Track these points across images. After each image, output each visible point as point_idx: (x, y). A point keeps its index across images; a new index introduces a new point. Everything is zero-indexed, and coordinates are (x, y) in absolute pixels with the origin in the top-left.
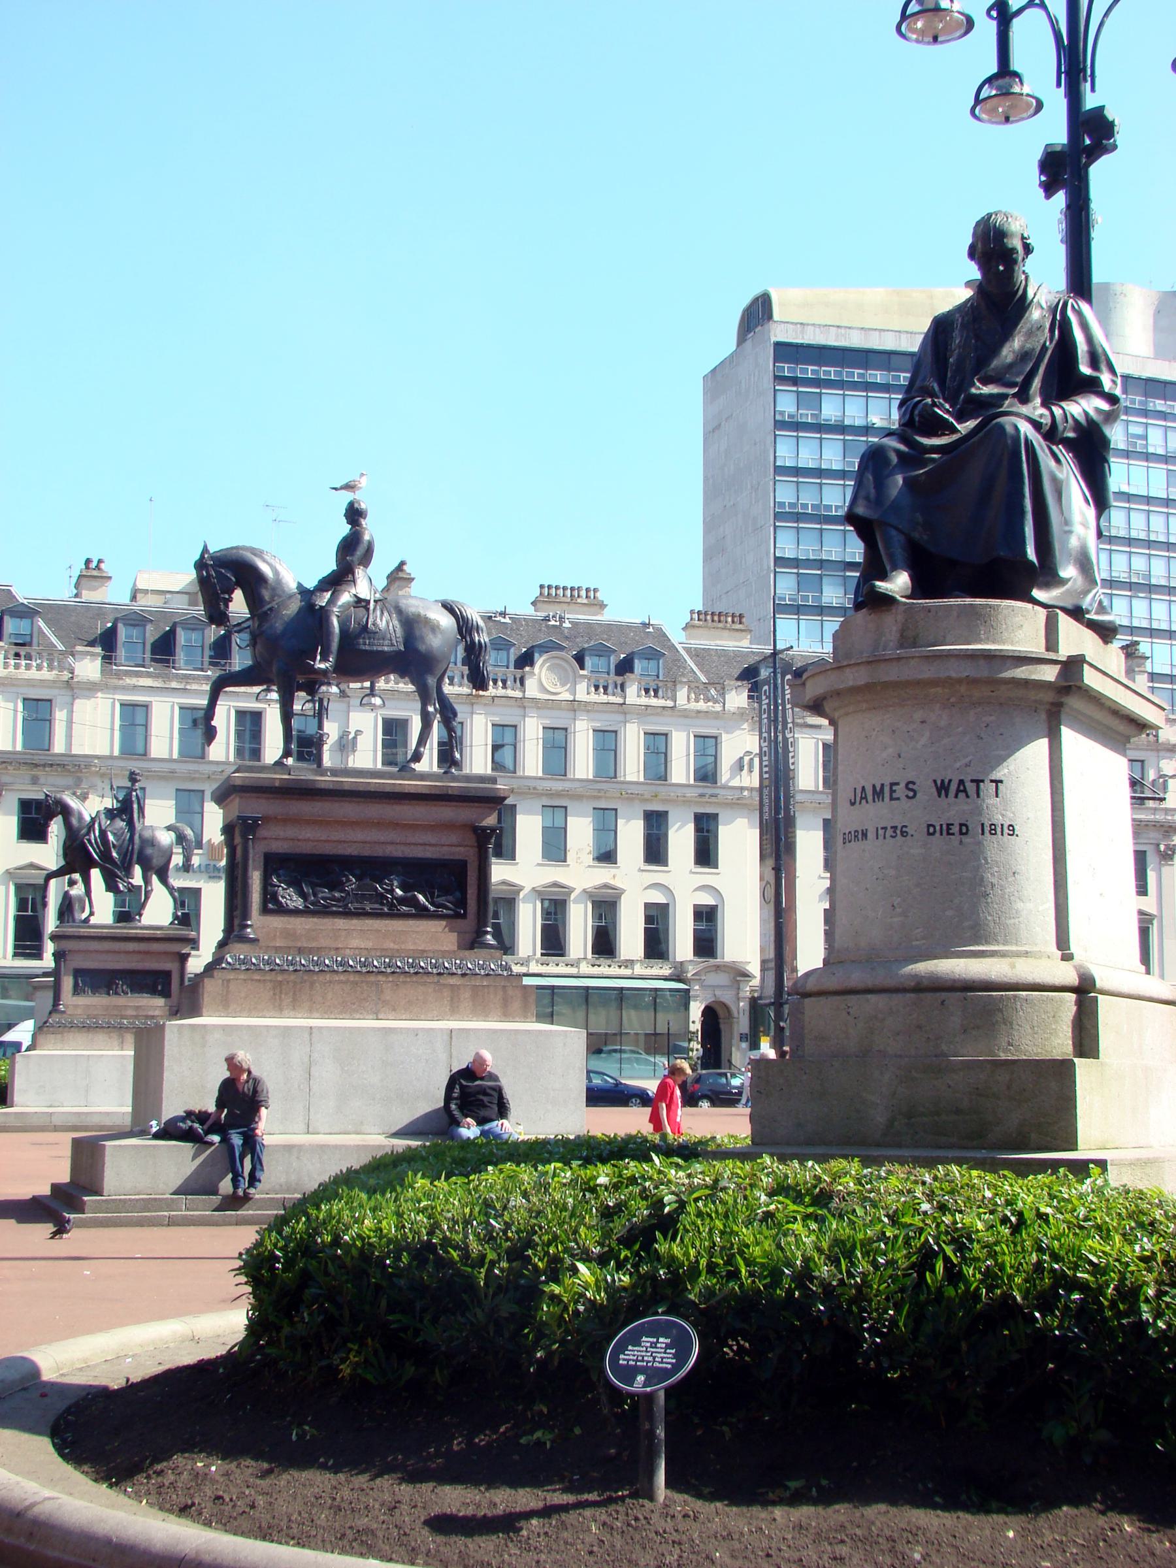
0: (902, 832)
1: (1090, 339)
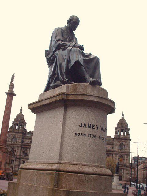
0: (94, 136)
1: (72, 83)
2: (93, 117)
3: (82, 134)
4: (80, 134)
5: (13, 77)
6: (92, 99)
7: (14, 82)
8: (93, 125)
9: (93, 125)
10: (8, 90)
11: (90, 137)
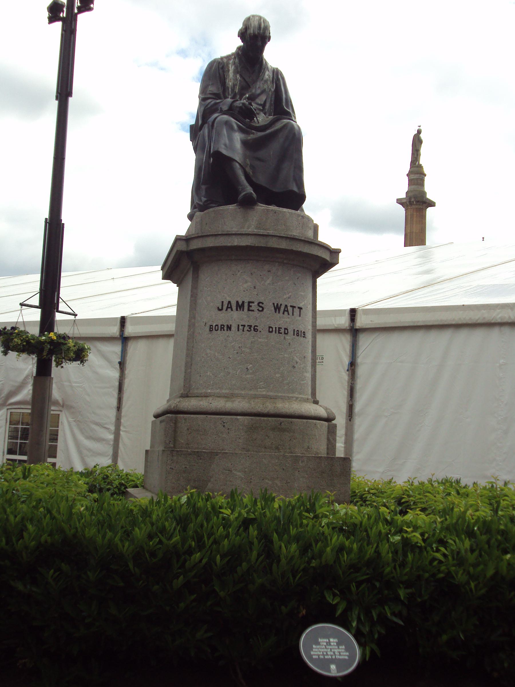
2: (249, 284)
3: (222, 327)
4: (219, 326)
5: (417, 142)
6: (236, 242)
7: (422, 161)
8: (249, 302)
9: (249, 302)
10: (406, 189)
11: (243, 331)
